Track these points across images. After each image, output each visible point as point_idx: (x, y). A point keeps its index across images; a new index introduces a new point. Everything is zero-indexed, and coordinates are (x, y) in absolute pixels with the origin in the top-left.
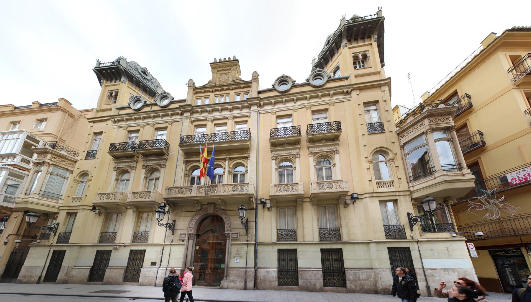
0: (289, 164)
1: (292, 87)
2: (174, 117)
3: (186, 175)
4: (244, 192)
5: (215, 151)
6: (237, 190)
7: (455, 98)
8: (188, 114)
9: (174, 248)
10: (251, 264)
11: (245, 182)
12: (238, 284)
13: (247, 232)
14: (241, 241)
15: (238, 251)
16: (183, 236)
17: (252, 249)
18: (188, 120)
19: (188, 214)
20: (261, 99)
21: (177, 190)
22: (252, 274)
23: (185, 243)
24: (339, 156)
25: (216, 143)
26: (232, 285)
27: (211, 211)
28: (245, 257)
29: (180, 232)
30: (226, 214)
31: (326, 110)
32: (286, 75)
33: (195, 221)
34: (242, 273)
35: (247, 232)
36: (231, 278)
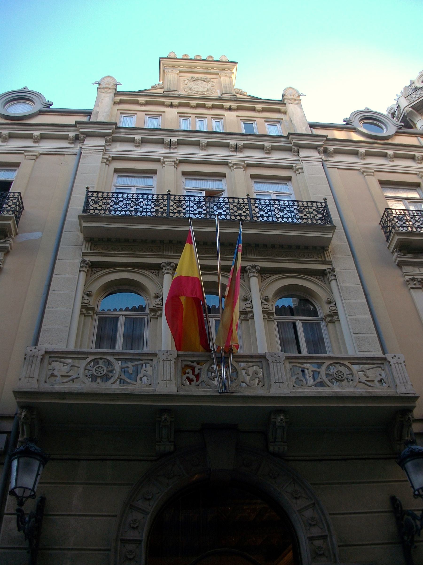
0: (226, 294)
1: (41, 113)
2: (47, 144)
3: (87, 310)
4: (137, 387)
5: (222, 244)
6: (106, 378)
8: (101, 142)
11: (147, 348)
18: (100, 155)
20: (328, 140)
21: (83, 364)
25: (253, 224)
31: (17, 165)
32: (30, 88)
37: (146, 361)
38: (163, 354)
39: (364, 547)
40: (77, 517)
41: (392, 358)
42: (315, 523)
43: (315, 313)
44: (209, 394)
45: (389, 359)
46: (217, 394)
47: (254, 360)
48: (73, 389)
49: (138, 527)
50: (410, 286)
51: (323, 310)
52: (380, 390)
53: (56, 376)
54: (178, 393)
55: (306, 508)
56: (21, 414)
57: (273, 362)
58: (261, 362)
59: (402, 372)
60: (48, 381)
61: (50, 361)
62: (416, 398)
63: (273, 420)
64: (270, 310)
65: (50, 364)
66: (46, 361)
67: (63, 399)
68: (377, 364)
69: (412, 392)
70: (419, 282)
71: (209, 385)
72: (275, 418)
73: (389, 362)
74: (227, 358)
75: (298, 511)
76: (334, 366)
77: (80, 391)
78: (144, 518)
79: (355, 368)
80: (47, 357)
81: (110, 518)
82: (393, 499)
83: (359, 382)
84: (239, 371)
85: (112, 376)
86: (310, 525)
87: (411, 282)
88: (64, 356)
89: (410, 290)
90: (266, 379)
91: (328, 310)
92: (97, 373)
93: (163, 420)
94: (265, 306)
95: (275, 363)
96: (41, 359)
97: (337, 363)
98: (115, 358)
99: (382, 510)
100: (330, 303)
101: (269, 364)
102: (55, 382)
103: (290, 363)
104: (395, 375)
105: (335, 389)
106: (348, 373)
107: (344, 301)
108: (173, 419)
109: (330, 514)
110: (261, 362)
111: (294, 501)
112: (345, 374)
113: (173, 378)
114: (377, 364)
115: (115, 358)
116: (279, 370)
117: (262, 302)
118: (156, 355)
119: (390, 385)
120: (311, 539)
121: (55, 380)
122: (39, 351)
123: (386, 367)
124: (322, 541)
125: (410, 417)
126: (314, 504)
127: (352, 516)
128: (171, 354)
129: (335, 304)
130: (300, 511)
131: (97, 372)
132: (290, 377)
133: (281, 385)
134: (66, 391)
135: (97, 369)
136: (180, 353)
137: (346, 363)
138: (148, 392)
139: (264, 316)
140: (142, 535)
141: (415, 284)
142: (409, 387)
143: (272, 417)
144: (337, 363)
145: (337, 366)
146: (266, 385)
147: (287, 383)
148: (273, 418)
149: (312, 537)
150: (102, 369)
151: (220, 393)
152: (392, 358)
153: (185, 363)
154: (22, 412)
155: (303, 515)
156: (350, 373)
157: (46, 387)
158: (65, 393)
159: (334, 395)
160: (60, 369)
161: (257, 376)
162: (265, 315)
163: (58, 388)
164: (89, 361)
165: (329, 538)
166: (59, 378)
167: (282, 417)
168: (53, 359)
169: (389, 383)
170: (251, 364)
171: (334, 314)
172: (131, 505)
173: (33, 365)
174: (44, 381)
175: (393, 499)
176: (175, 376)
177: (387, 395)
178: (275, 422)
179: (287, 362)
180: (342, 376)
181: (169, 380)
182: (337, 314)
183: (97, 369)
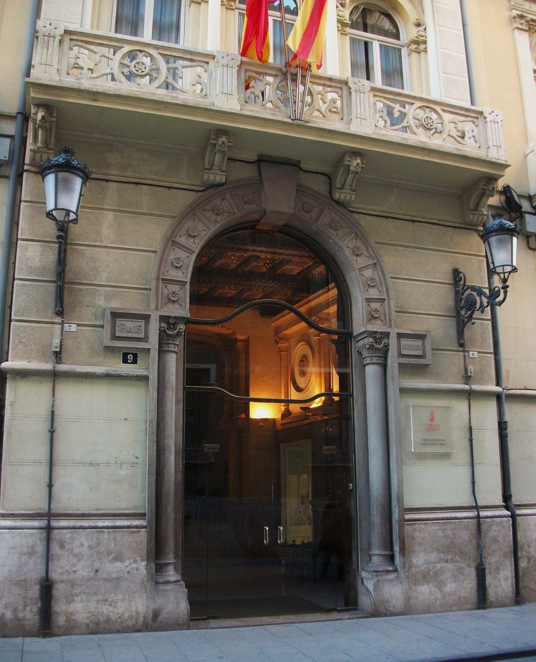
7: (176, 286)
9: (73, 398)
10: (491, 492)
12: (450, 587)
13: (460, 334)
14: (438, 376)
15: (431, 426)
16: (129, 327)
17: (486, 415)
19: (144, 197)
22: (499, 531)
23: (146, 367)
24: (459, 605)
26: (425, 592)
27: (279, 202)
28: (465, 457)
29: (104, 302)
30: (359, 234)
33: (197, 245)
34: (465, 536)
35: (460, 334)
36: (420, 559)
37: (200, 64)
38: (223, 57)
39: (419, 316)
40: (109, 250)
41: (490, 114)
42: (373, 284)
43: (397, 36)
44: (279, 119)
45: (486, 114)
46: (289, 121)
47: (333, 84)
48: (107, 88)
49: (181, 266)
50: (515, 25)
51: (408, 33)
52: (470, 148)
53: (82, 68)
54: (243, 112)
55: (367, 267)
56: (36, 114)
57: (356, 91)
58: (341, 88)
59: (497, 133)
60: (71, 72)
61: (72, 45)
62: (507, 166)
63: (347, 163)
64: (345, 19)
65: (71, 49)
66: (67, 43)
67: (95, 100)
68: (472, 117)
69: (503, 158)
70: (527, 22)
71: (277, 108)
72: (350, 161)
73: (485, 118)
74: (304, 77)
75: (358, 269)
76: (424, 110)
77: (117, 93)
78: (188, 257)
79: (447, 117)
80: (67, 38)
81: (148, 254)
82: (456, 272)
83: (449, 135)
84: (314, 95)
85: (156, 78)
86: (369, 285)
87: (518, 20)
88: (91, 40)
89: (514, 29)
90: (346, 111)
91: (416, 35)
92: (137, 71)
93: (220, 143)
94: (340, 13)
95: (358, 94)
96: (60, 40)
97: (428, 107)
98: (159, 53)
99: (443, 281)
100: (418, 25)
101: (351, 93)
102: (80, 76)
103: (375, 96)
104: (489, 135)
105: (421, 138)
106: (439, 121)
107: (437, 27)
108: (231, 144)
109: (391, 278)
110: (341, 88)
111: (355, 258)
112: (435, 123)
113: (235, 92)
114: (472, 117)
115: (159, 53)
116: (362, 103)
117: (337, 7)
118: (214, 57)
119: (481, 146)
120: (369, 300)
121: (81, 74)
122: (55, 28)
123: (480, 122)
124: (379, 304)
125: (495, 186)
126: (375, 264)
127: (413, 282)
128: (232, 59)
129: (425, 29)
130: (360, 269)
131: (136, 69)
132: (373, 114)
133: (363, 121)
134: (98, 91)
135: (137, 65)
136: (244, 59)
137: (438, 109)
138: (205, 106)
139: (338, 27)
140: (186, 275)
141: (522, 24)
142: (501, 152)
143: (347, 158)
144: (428, 107)
145: (427, 110)
146: (345, 118)
147: (370, 121)
148: (348, 161)
149: (370, 299)
150: (144, 66)
151: (292, 119)
152: (490, 114)
153: (249, 74)
154: (37, 112)
155: (362, 274)
156: (441, 122)
157: (69, 81)
158: (97, 93)
159: (420, 145)
160: (85, 57)
161: (335, 105)
162: (339, 25)
163: (86, 84)
164: (125, 52)
165: (386, 302)
166: (85, 71)
167: (359, 161)
168: (76, 43)
169: (480, 143)
170: (329, 89)
171: (422, 42)
172: (173, 241)
173: (50, 49)
174: (66, 73)
175: (456, 272)
176: (238, 89)
177: (477, 157)
178: (349, 166)
179: (372, 94)
180: (432, 124)
181: (231, 93)
182: (425, 42)
183: (137, 65)
